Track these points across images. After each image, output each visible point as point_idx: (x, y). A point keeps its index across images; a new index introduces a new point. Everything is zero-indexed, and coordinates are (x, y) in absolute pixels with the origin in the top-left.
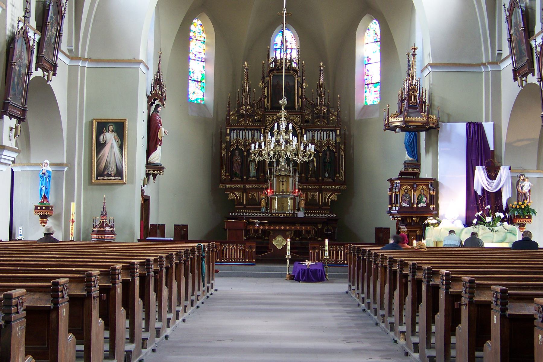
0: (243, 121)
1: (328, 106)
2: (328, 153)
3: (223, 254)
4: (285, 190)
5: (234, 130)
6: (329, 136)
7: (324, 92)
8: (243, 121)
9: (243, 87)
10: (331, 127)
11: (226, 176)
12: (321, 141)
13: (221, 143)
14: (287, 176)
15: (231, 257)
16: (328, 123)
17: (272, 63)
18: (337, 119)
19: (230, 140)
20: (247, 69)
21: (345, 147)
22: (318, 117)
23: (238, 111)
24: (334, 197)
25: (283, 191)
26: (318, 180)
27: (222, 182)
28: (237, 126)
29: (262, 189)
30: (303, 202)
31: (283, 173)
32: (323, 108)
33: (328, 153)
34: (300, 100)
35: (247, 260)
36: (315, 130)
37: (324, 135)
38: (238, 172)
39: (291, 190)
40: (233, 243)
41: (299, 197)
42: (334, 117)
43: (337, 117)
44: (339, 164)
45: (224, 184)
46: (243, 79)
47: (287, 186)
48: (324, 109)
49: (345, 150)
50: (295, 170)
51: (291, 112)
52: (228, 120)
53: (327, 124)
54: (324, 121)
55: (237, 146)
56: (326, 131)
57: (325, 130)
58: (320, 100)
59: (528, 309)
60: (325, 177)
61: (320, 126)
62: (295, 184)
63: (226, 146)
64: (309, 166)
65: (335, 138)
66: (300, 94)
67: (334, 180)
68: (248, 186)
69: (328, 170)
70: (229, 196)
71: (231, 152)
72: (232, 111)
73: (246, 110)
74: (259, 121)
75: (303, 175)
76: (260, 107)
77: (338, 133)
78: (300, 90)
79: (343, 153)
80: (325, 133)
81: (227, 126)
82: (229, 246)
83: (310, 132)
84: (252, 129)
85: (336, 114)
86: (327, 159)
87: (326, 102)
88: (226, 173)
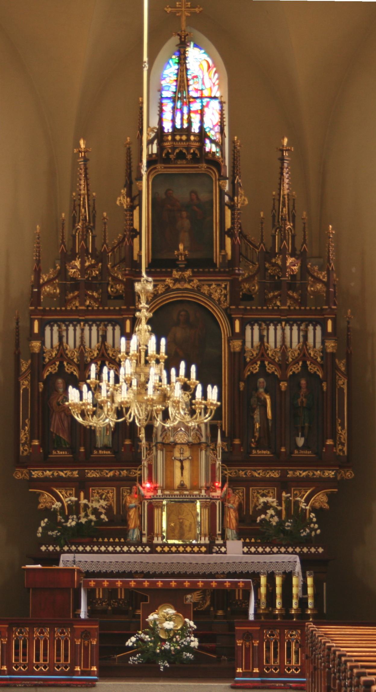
0: (75, 298)
1: (302, 257)
2: (303, 382)
3: (17, 654)
4: (187, 483)
5: (51, 323)
6: (306, 338)
7: (293, 218)
9: (75, 206)
10: (311, 312)
11: (31, 446)
12: (284, 349)
15: (38, 659)
16: (303, 301)
18: (328, 292)
19: (42, 350)
20: (86, 160)
21: (348, 365)
22: (277, 286)
23: (63, 274)
25: (182, 487)
26: (276, 453)
27: (21, 462)
28: (61, 313)
30: (232, 515)
32: (290, 260)
33: (303, 382)
34: (228, 241)
35: (78, 669)
36: (268, 321)
37: (294, 335)
38: (64, 436)
39: (203, 483)
40: (42, 625)
41: (224, 500)
42: (319, 286)
43: (327, 284)
45: (26, 467)
46: (74, 186)
48: (293, 264)
49: (348, 374)
51: (204, 274)
52: (35, 299)
53: (300, 304)
54: (291, 298)
55: (61, 366)
56: (298, 322)
57: (295, 321)
58: (281, 241)
60: (297, 448)
61: (280, 311)
62: (214, 465)
63: (31, 367)
64: (253, 418)
65: (323, 343)
66: (228, 224)
68: (92, 474)
69: (303, 428)
70: (41, 500)
72: (47, 272)
73: (83, 270)
74: (118, 297)
75: (237, 442)
76: (122, 261)
77: (330, 329)
78: (228, 213)
79: (342, 382)
80: (295, 328)
81: (32, 313)
82: (31, 632)
83: (256, 328)
84: (101, 321)
85: (323, 276)
86: (302, 400)
87: (298, 246)
88: (32, 438)
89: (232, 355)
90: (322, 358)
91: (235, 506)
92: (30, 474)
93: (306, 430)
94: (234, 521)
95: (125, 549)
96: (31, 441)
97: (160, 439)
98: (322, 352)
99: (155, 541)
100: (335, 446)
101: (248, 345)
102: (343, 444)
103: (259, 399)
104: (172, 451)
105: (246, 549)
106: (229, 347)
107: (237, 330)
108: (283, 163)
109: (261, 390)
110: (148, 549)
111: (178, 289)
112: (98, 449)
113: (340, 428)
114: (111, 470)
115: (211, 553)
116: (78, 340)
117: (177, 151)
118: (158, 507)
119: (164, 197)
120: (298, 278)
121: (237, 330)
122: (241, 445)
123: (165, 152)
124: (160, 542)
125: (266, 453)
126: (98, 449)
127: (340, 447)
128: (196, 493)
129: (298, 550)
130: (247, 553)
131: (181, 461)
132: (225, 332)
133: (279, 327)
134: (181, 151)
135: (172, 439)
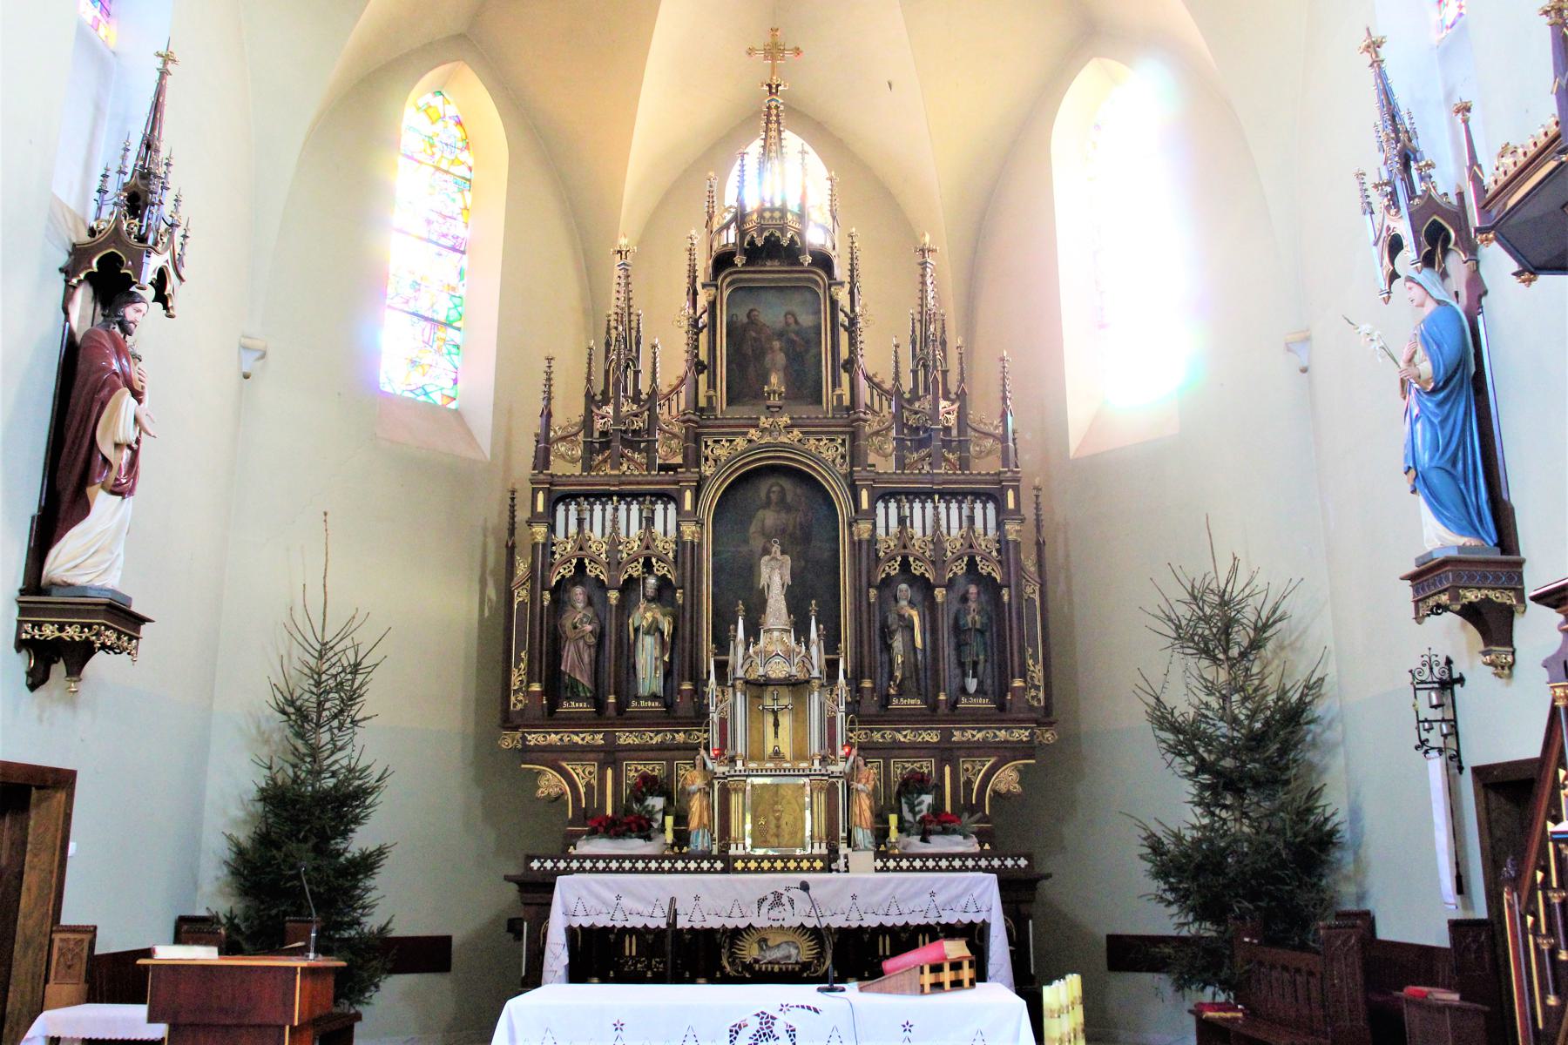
0: (605, 461)
5: (566, 498)
8: (605, 461)
11: (528, 694)
13: (511, 550)
14: (797, 686)
17: (727, 226)
24: (1007, 779)
26: (934, 706)
27: (509, 721)
29: (691, 749)
31: (778, 670)
38: (584, 679)
41: (849, 777)
44: (1021, 637)
47: (795, 731)
50: (832, 665)
54: (947, 460)
59: (331, 873)
67: (1002, 707)
68: (626, 738)
70: (542, 782)
71: (553, 591)
84: (644, 494)
86: (973, 617)
88: (530, 681)
89: (856, 546)
90: (999, 551)
91: (870, 787)
92: (524, 739)
93: (980, 668)
94: (867, 814)
95: (680, 865)
96: (528, 686)
97: (740, 673)
98: (998, 542)
99: (732, 851)
100: (1024, 689)
101: (881, 531)
102: (1037, 688)
103: (901, 617)
104: (760, 697)
105: (879, 864)
106: (851, 534)
107: (865, 505)
108: (924, 269)
109: (904, 603)
110: (719, 865)
111: (768, 445)
112: (637, 698)
113: (1030, 662)
114: (658, 733)
115: (831, 871)
116: (608, 524)
117: (766, 234)
118: (736, 790)
119: (745, 320)
120: (954, 432)
121: (865, 505)
122: (873, 690)
123: (748, 238)
124: (740, 852)
125: (914, 703)
126: (637, 698)
127: (1033, 693)
128: (804, 765)
129: (996, 863)
130: (882, 870)
131: (775, 713)
132: (844, 508)
133: (929, 505)
134: (772, 234)
135: (761, 671)
